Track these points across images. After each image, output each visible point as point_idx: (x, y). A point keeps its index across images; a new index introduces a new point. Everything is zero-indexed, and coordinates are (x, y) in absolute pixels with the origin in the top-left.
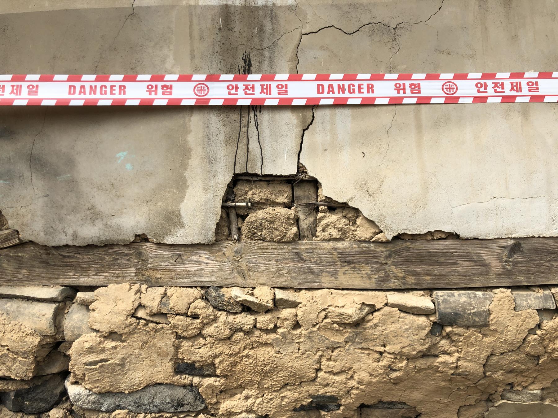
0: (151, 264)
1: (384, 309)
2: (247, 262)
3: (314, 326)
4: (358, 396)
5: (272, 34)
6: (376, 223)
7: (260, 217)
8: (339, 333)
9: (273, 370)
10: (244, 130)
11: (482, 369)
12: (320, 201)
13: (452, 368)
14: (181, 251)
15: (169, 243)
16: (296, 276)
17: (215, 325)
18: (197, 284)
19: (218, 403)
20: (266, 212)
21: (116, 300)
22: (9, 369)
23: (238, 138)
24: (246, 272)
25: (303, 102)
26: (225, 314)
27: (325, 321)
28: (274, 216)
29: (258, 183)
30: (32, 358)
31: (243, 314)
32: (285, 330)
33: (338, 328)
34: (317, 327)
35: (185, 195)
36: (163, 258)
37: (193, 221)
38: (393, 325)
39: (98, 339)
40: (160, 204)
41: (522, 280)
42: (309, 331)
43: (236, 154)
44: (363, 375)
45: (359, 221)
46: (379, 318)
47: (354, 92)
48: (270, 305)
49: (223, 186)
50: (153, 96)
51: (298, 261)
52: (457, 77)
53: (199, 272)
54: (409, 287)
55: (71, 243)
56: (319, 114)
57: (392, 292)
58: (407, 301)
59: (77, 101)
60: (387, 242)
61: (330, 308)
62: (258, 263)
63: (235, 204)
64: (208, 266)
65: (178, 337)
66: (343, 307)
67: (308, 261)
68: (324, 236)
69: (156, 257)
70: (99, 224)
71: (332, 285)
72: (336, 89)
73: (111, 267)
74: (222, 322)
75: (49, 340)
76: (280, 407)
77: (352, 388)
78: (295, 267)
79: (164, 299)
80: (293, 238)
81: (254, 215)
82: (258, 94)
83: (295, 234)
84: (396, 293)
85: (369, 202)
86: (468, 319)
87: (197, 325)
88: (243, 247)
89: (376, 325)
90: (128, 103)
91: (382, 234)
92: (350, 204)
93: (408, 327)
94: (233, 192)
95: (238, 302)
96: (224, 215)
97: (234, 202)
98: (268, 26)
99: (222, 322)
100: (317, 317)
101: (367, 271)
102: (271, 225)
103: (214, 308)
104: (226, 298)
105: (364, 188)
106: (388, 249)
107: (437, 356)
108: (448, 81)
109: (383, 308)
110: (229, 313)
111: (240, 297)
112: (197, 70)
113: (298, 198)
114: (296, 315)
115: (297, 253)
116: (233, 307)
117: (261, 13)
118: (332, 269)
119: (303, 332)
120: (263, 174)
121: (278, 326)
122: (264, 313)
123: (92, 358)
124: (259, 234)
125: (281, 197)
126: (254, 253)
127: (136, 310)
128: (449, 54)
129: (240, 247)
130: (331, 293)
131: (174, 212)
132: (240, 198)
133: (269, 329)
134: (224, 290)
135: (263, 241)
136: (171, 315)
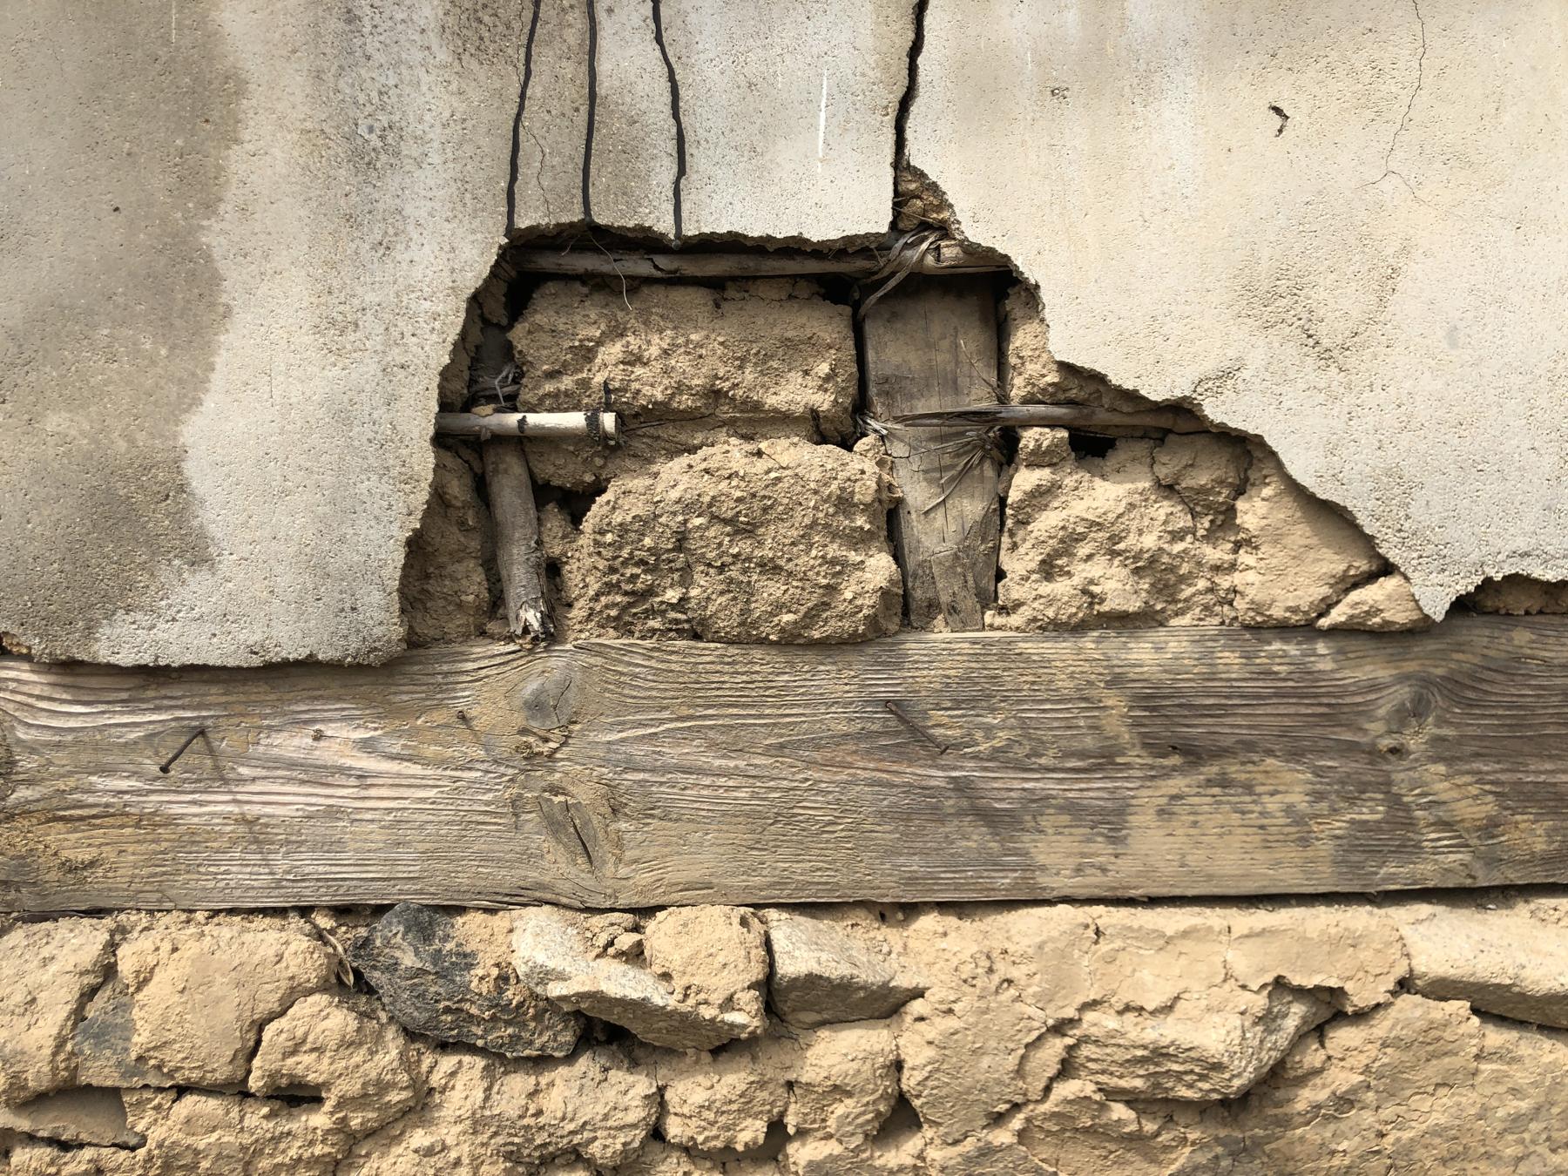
0: (30, 783)
1: (1393, 1012)
2: (605, 762)
3: (998, 1119)
6: (1362, 519)
7: (674, 495)
8: (1137, 1151)
12: (1026, 401)
14: (207, 707)
15: (126, 659)
16: (886, 834)
17: (419, 1138)
18: (309, 898)
20: (712, 464)
23: (528, 15)
24: (596, 820)
26: (477, 1072)
27: (1068, 1089)
28: (757, 487)
29: (659, 293)
31: (584, 1063)
32: (833, 1148)
33: (1133, 1127)
34: (1017, 1122)
35: (211, 368)
36: (96, 747)
37: (260, 526)
38: (1445, 1098)
40: (54, 421)
42: (969, 1145)
43: (521, 107)
45: (1253, 512)
46: (1364, 1060)
48: (746, 1017)
49: (440, 308)
51: (899, 753)
53: (320, 828)
54: (1515, 876)
57: (1423, 909)
58: (1522, 959)
60: (1422, 628)
61: (1090, 1016)
62: (666, 770)
63: (522, 421)
64: (373, 792)
66: (1168, 1009)
67: (957, 746)
68: (1050, 603)
69: (58, 746)
71: (1092, 882)
74: (459, 1120)
78: (880, 783)
79: (100, 1000)
80: (872, 621)
81: (639, 483)
83: (885, 593)
84: (1440, 909)
85: (1321, 397)
87: (312, 1143)
88: (578, 676)
89: (1345, 1102)
91: (1389, 584)
92: (1216, 411)
93: (1524, 1105)
94: (509, 347)
95: (552, 1004)
96: (458, 490)
97: (515, 410)
99: (459, 1120)
100: (1020, 1072)
101: (1289, 799)
102: (743, 546)
103: (411, 1034)
104: (480, 979)
105: (1289, 317)
106: (1411, 667)
109: (1388, 1005)
110: (500, 1061)
111: (562, 977)
113: (893, 387)
114: (898, 1065)
115: (897, 703)
116: (524, 1025)
118: (1094, 790)
119: (933, 1154)
120: (690, 230)
121: (791, 1130)
122: (706, 1057)
124: (672, 595)
125: (796, 377)
126: (639, 709)
129: (557, 675)
130: (1098, 932)
131: (147, 469)
132: (549, 387)
133: (740, 1148)
134: (470, 928)
135: (697, 637)
136: (147, 1095)
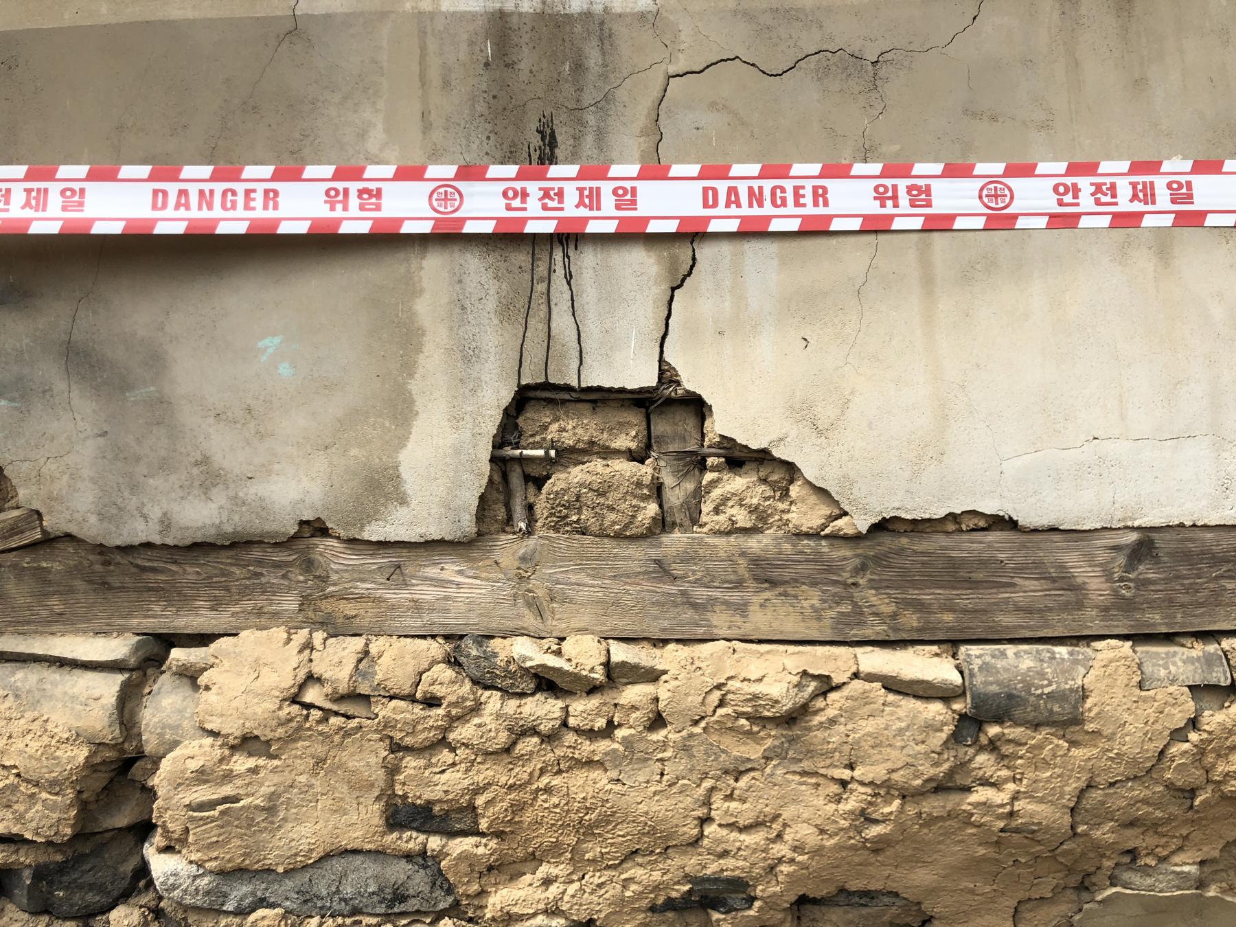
0: (334, 585)
1: (850, 686)
2: (548, 581)
3: (696, 723)
4: (793, 879)
5: (604, 76)
6: (833, 494)
7: (576, 480)
8: (752, 739)
9: (605, 820)
10: (541, 288)
11: (1067, 819)
12: (709, 447)
13: (1000, 817)
14: (402, 557)
15: (374, 538)
16: (655, 611)
17: (476, 721)
18: (436, 630)
19: (482, 893)
20: (590, 470)
21: (257, 665)
22: (19, 819)
23: (526, 306)
24: (545, 603)
25: (671, 227)
26: (498, 697)
27: (721, 711)
28: (606, 478)
29: (572, 405)
30: (70, 794)
31: (538, 696)
32: (632, 731)
33: (748, 728)
34: (703, 724)
35: (410, 433)
36: (360, 572)
37: (427, 490)
38: (871, 721)
39: (218, 753)
40: (354, 452)
41: (1157, 621)
42: (684, 733)
43: (524, 340)
44: (804, 832)
45: (795, 490)
46: (839, 704)
47: (784, 204)
48: (599, 675)
49: (493, 413)
50: (339, 213)
51: (660, 580)
52: (1012, 171)
53: (441, 604)
54: (905, 636)
55: (157, 539)
56: (706, 253)
57: (869, 648)
58: (902, 666)
59: (171, 224)
60: (858, 538)
61: (730, 683)
62: (571, 584)
63: (521, 453)
64: (462, 590)
65: (395, 747)
66: (760, 680)
67: (681, 578)
68: (717, 524)
69: (346, 571)
70: (220, 497)
71: (735, 632)
72: (744, 198)
73: (245, 592)
74: (491, 714)
75: (109, 754)
76: (621, 902)
77: (780, 860)
78: (653, 591)
79: (364, 662)
80: (649, 529)
81: (563, 476)
82: (571, 208)
83: (654, 519)
84: (876, 649)
85: (818, 448)
86: (1036, 708)
87: (437, 720)
88: (539, 548)
89: (833, 722)
90: (284, 229)
91: (845, 519)
92: (776, 453)
93: (903, 725)
94: (516, 425)
95: (527, 670)
96: (497, 478)
97: (518, 448)
98: (593, 59)
99: (491, 714)
100: (703, 703)
101: (812, 602)
102: (601, 500)
103: (475, 682)
104: (500, 661)
105: (806, 418)
106: (859, 551)
107: (967, 789)
108: (993, 179)
109: (848, 683)
110: (507, 693)
111: (531, 659)
112: (436, 156)
113: (661, 440)
114: (657, 700)
115: (659, 561)
116: (516, 680)
117: (578, 29)
118: (735, 596)
119: (670, 736)
120: (584, 385)
121: (616, 723)
122: (584, 694)
123: (203, 794)
124: (574, 518)
125: (623, 436)
126: (562, 561)
127: (302, 687)
128: (994, 119)
129: (531, 547)
130: (734, 650)
131: (386, 469)
132: (531, 440)
133: (596, 729)
134: (496, 644)
135: (584, 534)
136: (380, 698)
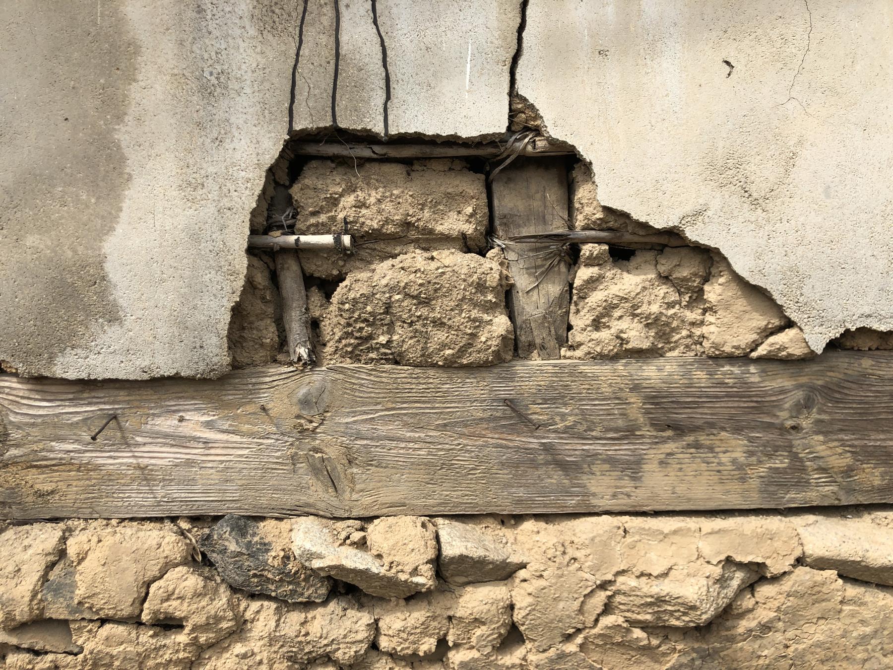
0: (17, 446)
1: (793, 577)
2: (344, 434)
3: (568, 638)
6: (776, 296)
7: (384, 282)
8: (648, 656)
12: (585, 228)
14: (118, 403)
15: (72, 375)
16: (505, 475)
17: (239, 648)
18: (176, 512)
20: (406, 265)
23: (301, 9)
24: (339, 467)
26: (272, 611)
27: (608, 620)
28: (431, 277)
29: (375, 167)
31: (332, 605)
32: (475, 654)
33: (645, 642)
34: (579, 639)
35: (120, 210)
36: (55, 426)
37: (148, 300)
38: (823, 626)
40: (31, 240)
42: (552, 653)
43: (297, 61)
45: (713, 292)
46: (777, 604)
48: (425, 579)
49: (251, 176)
51: (512, 429)
53: (182, 472)
54: (863, 499)
57: (811, 518)
58: (867, 546)
60: (810, 358)
61: (621, 579)
62: (379, 438)
63: (298, 240)
64: (212, 451)
66: (665, 575)
67: (545, 425)
68: (598, 344)
69: (33, 425)
71: (622, 503)
74: (261, 638)
78: (501, 446)
79: (57, 570)
80: (497, 354)
81: (364, 275)
83: (504, 338)
84: (820, 518)
85: (753, 226)
87: (177, 651)
88: (329, 385)
89: (766, 628)
91: (791, 333)
92: (692, 234)
93: (868, 630)
94: (290, 197)
95: (314, 572)
96: (261, 279)
97: (293, 233)
99: (261, 638)
100: (581, 611)
101: (734, 455)
102: (423, 311)
103: (234, 589)
104: (273, 558)
105: (734, 181)
106: (804, 380)
109: (790, 573)
110: (285, 604)
111: (320, 557)
113: (509, 220)
114: (512, 607)
115: (511, 400)
116: (298, 584)
118: (623, 450)
119: (531, 657)
120: (393, 131)
121: (451, 644)
122: (402, 602)
124: (383, 339)
125: (453, 215)
126: (364, 404)
129: (317, 384)
130: (625, 531)
131: (83, 267)
132: (313, 220)
133: (421, 654)
134: (268, 529)
135: (397, 363)
136: (84, 624)
